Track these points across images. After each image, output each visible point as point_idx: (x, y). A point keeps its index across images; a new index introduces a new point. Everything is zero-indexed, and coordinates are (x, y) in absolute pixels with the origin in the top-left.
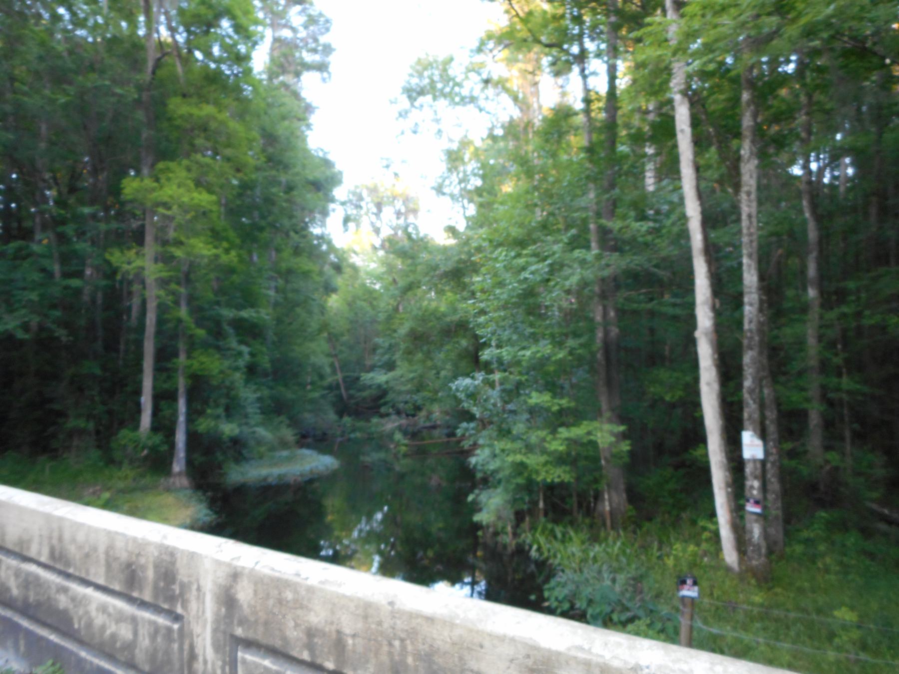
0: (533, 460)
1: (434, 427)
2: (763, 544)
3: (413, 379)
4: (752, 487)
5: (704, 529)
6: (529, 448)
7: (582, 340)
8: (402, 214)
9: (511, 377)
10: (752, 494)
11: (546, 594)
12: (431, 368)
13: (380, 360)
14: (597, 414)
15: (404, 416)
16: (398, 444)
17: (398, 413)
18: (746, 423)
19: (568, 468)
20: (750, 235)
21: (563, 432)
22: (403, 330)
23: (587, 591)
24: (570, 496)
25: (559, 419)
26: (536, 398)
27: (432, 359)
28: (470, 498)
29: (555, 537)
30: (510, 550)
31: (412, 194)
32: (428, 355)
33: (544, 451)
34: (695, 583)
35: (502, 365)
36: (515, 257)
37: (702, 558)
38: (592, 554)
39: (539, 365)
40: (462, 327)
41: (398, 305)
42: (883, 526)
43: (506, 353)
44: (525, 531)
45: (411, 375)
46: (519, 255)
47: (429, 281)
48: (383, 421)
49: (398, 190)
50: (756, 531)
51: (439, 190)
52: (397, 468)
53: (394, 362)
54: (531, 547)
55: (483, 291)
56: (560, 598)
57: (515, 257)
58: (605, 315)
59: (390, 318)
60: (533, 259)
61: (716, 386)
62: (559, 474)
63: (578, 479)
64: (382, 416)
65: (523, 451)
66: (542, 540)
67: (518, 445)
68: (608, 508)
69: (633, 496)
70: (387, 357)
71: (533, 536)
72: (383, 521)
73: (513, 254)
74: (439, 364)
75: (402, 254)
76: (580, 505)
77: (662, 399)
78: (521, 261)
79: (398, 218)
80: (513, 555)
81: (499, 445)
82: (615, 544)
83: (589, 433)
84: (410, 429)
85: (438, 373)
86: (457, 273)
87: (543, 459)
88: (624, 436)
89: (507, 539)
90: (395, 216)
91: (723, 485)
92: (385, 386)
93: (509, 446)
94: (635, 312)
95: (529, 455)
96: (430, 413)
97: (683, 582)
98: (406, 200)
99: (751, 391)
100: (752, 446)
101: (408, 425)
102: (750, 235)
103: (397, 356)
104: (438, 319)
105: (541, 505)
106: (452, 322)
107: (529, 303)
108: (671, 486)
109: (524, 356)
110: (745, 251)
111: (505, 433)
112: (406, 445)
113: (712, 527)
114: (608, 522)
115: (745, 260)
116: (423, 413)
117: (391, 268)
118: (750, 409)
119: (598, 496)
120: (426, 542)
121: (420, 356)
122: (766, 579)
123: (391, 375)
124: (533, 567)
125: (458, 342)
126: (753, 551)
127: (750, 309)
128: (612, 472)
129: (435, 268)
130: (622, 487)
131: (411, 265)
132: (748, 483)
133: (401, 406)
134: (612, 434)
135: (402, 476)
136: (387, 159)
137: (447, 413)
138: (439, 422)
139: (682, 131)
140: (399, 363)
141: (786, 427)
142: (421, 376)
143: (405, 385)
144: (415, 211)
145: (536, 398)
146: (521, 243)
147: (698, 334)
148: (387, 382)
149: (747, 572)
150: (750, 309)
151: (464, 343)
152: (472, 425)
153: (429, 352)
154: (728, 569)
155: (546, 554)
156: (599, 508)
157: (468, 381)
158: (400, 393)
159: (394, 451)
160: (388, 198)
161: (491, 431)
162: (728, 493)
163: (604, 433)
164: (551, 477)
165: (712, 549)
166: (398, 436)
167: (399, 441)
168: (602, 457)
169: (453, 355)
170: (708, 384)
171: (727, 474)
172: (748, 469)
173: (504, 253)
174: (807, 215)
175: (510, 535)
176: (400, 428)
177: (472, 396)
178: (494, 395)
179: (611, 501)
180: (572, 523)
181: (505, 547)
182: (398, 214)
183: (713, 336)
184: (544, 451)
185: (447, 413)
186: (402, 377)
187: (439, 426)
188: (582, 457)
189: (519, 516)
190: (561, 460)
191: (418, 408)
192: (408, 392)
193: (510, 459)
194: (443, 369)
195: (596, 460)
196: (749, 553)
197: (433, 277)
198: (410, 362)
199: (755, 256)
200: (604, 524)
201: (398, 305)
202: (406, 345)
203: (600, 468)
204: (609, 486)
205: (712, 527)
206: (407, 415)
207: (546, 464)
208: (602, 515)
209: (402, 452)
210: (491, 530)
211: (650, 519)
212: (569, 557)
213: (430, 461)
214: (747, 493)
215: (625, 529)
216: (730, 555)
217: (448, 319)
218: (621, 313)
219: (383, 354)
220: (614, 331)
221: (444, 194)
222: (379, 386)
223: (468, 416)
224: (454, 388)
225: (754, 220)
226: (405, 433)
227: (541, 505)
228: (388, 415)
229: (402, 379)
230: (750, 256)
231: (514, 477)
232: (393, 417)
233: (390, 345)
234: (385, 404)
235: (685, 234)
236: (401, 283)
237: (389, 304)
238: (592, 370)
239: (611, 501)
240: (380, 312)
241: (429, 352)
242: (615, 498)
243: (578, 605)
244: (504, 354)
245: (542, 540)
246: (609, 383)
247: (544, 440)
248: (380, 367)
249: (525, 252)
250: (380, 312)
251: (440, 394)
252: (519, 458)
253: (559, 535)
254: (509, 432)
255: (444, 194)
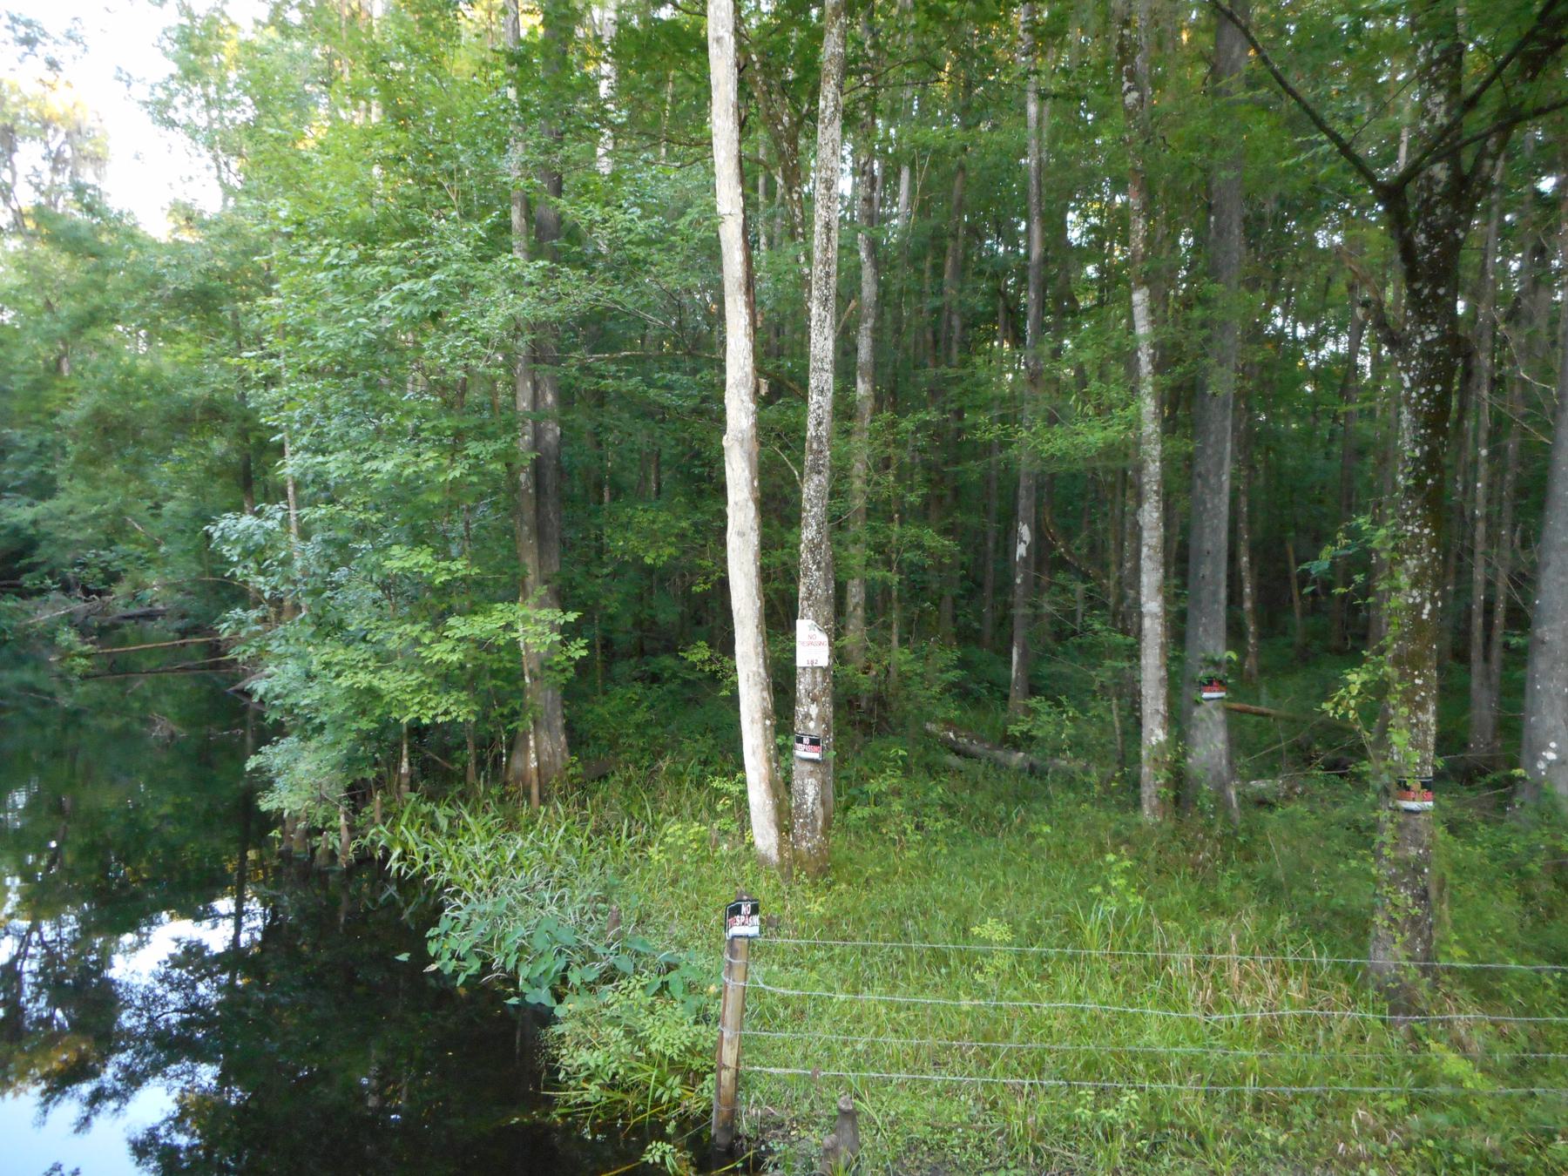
0: (390, 682)
1: (150, 616)
2: (820, 812)
3: (97, 516)
4: (807, 716)
5: (719, 794)
6: (385, 659)
7: (498, 445)
8: (66, 161)
9: (349, 514)
10: (806, 728)
11: (432, 948)
12: (141, 495)
13: (16, 476)
14: (514, 592)
15: (79, 593)
16: (67, 653)
17: (66, 588)
18: (802, 605)
19: (463, 696)
20: (827, 263)
21: (459, 626)
22: (77, 411)
23: (516, 933)
24: (462, 746)
25: (437, 603)
26: (402, 559)
27: (142, 477)
28: (251, 764)
29: (434, 827)
30: (342, 864)
31: (89, 122)
32: (136, 469)
33: (417, 663)
34: (755, 910)
35: (324, 490)
36: (358, 263)
37: (717, 845)
38: (510, 855)
39: (403, 492)
40: (214, 413)
41: (58, 361)
42: (953, 760)
43: (335, 465)
44: (372, 822)
45: (94, 510)
46: (366, 260)
47: (140, 308)
48: (26, 605)
49: (56, 105)
50: (809, 789)
51: (161, 113)
52: (66, 702)
53: (53, 479)
54: (387, 853)
55: (283, 331)
56: (462, 951)
57: (358, 263)
58: (536, 400)
59: (38, 388)
60: (396, 271)
61: (754, 539)
62: (455, 708)
63: (484, 717)
64: (25, 594)
65: (372, 664)
66: (411, 837)
67: (359, 653)
68: (534, 765)
69: (576, 739)
70: (33, 468)
71: (392, 829)
72: (31, 807)
73: (354, 254)
74: (161, 490)
75: (73, 242)
76: (481, 763)
77: (638, 559)
78: (373, 272)
79: (55, 170)
80: (351, 871)
81: (317, 656)
82: (551, 833)
83: (509, 627)
84: (95, 622)
85: (157, 506)
86: (206, 301)
87: (413, 679)
88: (569, 632)
89: (339, 841)
90: (48, 165)
91: (758, 716)
92: (31, 531)
93: (341, 654)
94: (601, 398)
95: (386, 673)
96: (140, 586)
97: (736, 911)
98: (75, 133)
99: (814, 548)
100: (812, 646)
101: (88, 614)
102: (827, 263)
103: (59, 470)
104: (164, 391)
105: (405, 767)
106: (192, 401)
107: (368, 371)
108: (640, 716)
109: (376, 471)
110: (815, 293)
111: (329, 627)
112: (87, 656)
113: (735, 789)
114: (535, 791)
115: (815, 309)
116: (121, 590)
117: (38, 276)
118: (812, 582)
119: (515, 742)
120: (136, 839)
121: (115, 469)
122: (824, 870)
123: (42, 507)
124: (392, 890)
125: (205, 444)
126: (804, 825)
127: (819, 402)
128: (541, 697)
129: (155, 282)
130: (560, 723)
131: (96, 269)
132: (800, 710)
133: (70, 573)
134: (553, 627)
135: (73, 718)
136: (29, 24)
137: (178, 588)
138: (159, 607)
139: (718, 40)
140: (63, 482)
141: (868, 611)
142: (119, 512)
143: (79, 530)
144: (97, 160)
145: (402, 559)
146: (366, 235)
147: (727, 441)
148: (34, 523)
149: (791, 864)
150: (819, 402)
151: (218, 446)
152: (254, 614)
153: (138, 462)
154: (763, 861)
155: (420, 864)
156: (517, 763)
157: (247, 520)
158: (67, 544)
159: (58, 669)
160: (31, 120)
161: (298, 627)
162: (765, 728)
163: (534, 627)
164: (431, 713)
165: (734, 828)
166: (67, 636)
167: (69, 648)
168: (526, 670)
169: (193, 469)
170: (741, 534)
171: (765, 694)
172: (803, 685)
173: (334, 251)
174: (863, 255)
175: (345, 834)
176: (70, 619)
177: (255, 553)
178: (305, 555)
179: (542, 749)
180: (464, 797)
181: (332, 855)
182: (57, 161)
183: (753, 447)
184: (417, 663)
185: (178, 588)
186: (71, 512)
187: (162, 614)
188: (493, 676)
189: (358, 795)
190: (447, 679)
191: (113, 578)
192: (88, 544)
193: (345, 682)
194: (170, 498)
195: (514, 677)
196: (798, 830)
197: (148, 300)
198: (91, 480)
199: (832, 303)
200: (528, 795)
201: (58, 361)
202: (80, 446)
203: (521, 692)
204: (535, 722)
205: (735, 789)
206: (87, 592)
207: (419, 689)
208: (521, 777)
209: (78, 671)
210: (301, 825)
211: (603, 777)
212: (466, 866)
213: (141, 684)
214: (799, 727)
215: (564, 799)
216: (764, 835)
217: (186, 393)
218: (566, 397)
219: (25, 464)
220: (553, 432)
221: (172, 124)
222: (16, 531)
223: (239, 595)
224: (216, 535)
225: (834, 235)
226: (84, 631)
227: (405, 767)
228: (41, 592)
229: (72, 517)
230: (824, 303)
231: (353, 719)
232: (53, 596)
233: (41, 444)
234: (31, 568)
235: (712, 250)
236: (68, 308)
237: (36, 357)
238: (514, 510)
239: (542, 749)
240: (12, 372)
241: (138, 462)
242: (547, 745)
243: (498, 960)
244: (332, 466)
245: (411, 837)
246: (540, 532)
247: (417, 641)
248: (15, 489)
249: (381, 253)
250: (12, 372)
251: (163, 549)
252: (363, 679)
253: (444, 824)
254: (340, 626)
255: (172, 124)
